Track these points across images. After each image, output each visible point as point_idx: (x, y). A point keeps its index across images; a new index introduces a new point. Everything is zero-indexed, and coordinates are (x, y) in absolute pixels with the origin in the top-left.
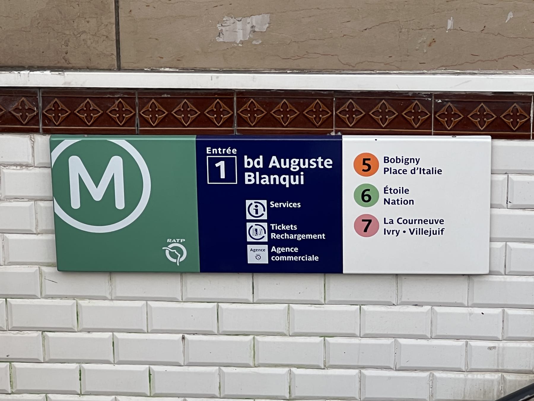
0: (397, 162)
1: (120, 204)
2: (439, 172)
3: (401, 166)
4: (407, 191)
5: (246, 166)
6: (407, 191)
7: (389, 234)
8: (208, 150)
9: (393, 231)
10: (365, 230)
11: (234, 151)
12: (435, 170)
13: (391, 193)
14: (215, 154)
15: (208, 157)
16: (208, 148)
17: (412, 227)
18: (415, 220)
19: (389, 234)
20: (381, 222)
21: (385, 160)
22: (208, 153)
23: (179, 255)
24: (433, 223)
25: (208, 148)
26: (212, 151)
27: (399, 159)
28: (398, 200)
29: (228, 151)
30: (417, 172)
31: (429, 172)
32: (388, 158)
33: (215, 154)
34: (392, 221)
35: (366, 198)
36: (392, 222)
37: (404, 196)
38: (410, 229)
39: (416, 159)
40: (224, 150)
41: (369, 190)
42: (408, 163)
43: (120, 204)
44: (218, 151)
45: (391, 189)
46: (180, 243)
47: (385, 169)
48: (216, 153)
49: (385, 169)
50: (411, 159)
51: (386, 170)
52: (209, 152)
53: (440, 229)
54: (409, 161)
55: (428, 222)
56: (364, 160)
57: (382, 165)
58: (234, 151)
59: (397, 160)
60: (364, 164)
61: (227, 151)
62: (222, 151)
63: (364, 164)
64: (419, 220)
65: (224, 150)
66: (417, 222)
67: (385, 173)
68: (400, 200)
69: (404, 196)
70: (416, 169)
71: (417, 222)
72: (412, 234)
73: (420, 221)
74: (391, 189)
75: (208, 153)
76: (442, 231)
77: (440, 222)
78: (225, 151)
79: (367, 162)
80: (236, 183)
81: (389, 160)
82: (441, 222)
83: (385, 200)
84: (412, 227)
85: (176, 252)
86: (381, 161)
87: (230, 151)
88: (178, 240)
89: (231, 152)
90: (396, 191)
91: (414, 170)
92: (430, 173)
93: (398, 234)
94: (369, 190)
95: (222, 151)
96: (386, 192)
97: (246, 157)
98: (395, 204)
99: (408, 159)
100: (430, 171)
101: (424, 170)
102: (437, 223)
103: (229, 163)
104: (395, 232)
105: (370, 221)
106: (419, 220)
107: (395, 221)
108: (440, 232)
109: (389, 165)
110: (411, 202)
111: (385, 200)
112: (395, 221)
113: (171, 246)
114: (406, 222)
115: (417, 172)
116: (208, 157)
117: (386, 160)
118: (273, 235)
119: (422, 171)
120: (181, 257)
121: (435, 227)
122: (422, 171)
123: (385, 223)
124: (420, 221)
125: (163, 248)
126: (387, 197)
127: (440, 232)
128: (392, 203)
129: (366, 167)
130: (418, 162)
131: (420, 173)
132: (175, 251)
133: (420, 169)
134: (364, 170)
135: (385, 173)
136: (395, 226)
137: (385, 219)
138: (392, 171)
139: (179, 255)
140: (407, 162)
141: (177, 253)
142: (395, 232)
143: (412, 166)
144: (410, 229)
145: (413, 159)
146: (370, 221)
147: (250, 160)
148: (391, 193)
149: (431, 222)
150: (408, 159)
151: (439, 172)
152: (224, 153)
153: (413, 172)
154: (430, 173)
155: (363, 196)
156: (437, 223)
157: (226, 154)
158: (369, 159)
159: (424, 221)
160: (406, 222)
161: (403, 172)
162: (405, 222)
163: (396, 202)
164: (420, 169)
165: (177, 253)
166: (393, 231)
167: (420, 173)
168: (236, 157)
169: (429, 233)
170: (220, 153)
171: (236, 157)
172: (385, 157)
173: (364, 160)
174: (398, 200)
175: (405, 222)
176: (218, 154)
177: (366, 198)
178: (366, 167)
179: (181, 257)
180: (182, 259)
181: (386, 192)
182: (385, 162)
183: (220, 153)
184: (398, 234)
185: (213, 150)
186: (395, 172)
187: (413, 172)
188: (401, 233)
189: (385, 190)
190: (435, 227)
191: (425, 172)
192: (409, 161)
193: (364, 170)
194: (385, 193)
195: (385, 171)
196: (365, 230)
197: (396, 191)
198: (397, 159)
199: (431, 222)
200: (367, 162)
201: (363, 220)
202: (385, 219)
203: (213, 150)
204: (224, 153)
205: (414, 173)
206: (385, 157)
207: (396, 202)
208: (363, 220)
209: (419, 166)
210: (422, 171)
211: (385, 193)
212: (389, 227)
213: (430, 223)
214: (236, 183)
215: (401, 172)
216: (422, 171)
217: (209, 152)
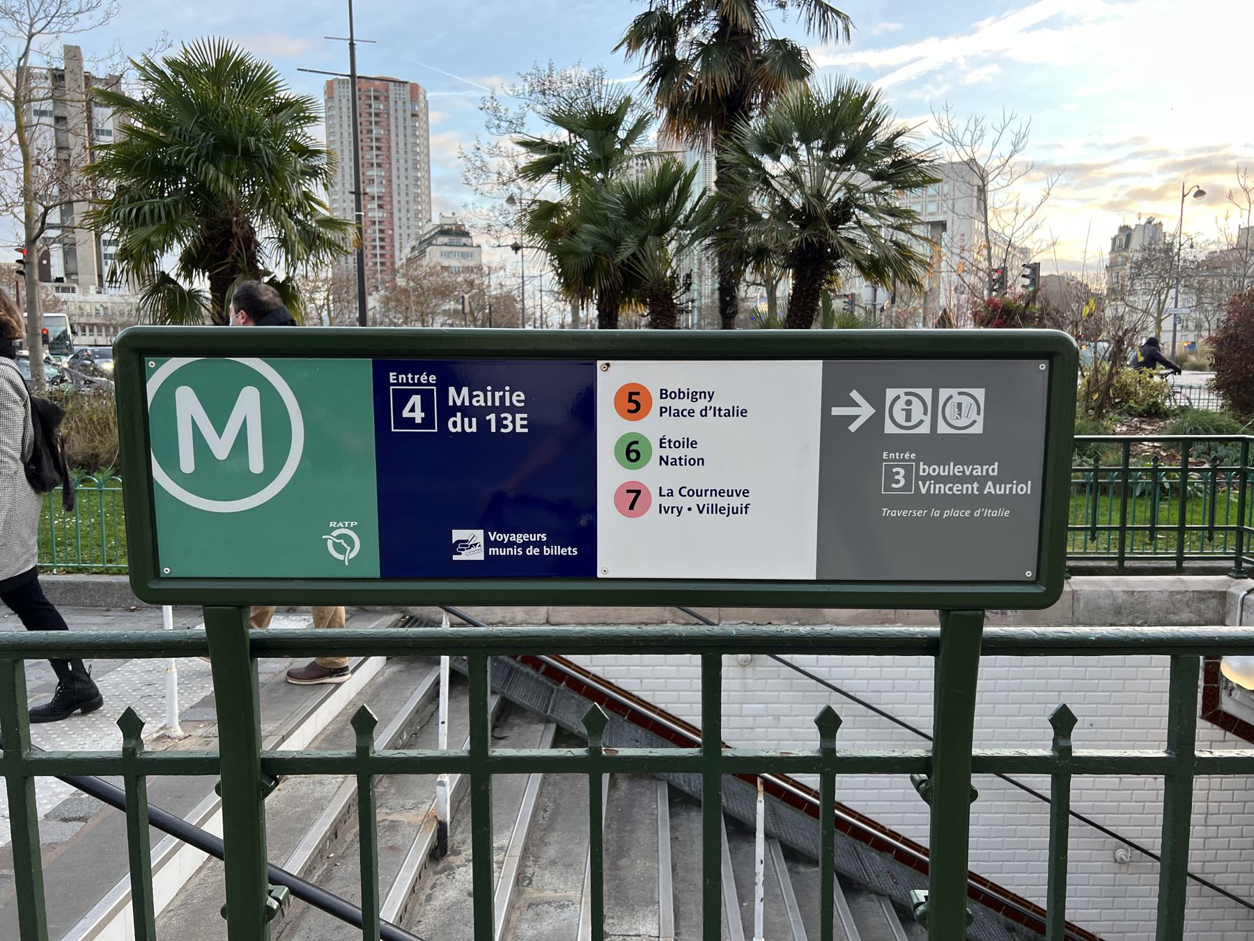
0: (679, 398)
1: (256, 464)
2: (743, 413)
3: (686, 404)
4: (694, 444)
5: (921, 473)
6: (694, 444)
7: (666, 512)
8: (391, 377)
9: (673, 508)
10: (631, 507)
11: (433, 378)
13: (670, 447)
14: (403, 384)
15: (391, 388)
16: (391, 374)
17: (702, 501)
18: (706, 491)
19: (666, 512)
20: (655, 493)
21: (662, 394)
22: (392, 381)
23: (349, 548)
24: (732, 496)
25: (391, 374)
26: (397, 379)
27: (683, 392)
28: (680, 459)
29: (424, 378)
30: (710, 413)
31: (728, 414)
32: (667, 391)
33: (403, 384)
34: (672, 493)
35: (633, 456)
36: (671, 494)
37: (690, 453)
38: (698, 505)
39: (709, 393)
40: (416, 377)
41: (636, 443)
42: (697, 399)
43: (256, 464)
44: (407, 379)
45: (670, 441)
46: (349, 528)
47: (661, 408)
48: (405, 381)
49: (661, 408)
50: (701, 393)
51: (664, 410)
52: (394, 379)
53: (744, 506)
54: (698, 396)
55: (726, 494)
56: (631, 394)
57: (657, 402)
58: (433, 378)
59: (680, 394)
60: (630, 400)
61: (422, 379)
62: (413, 379)
63: (630, 400)
64: (712, 491)
65: (416, 377)
66: (709, 493)
67: (661, 416)
68: (684, 458)
69: (690, 453)
70: (708, 408)
71: (709, 493)
72: (701, 512)
73: (714, 492)
74: (670, 441)
75: (392, 381)
76: (746, 507)
77: (744, 493)
78: (419, 379)
79: (634, 397)
80: (436, 431)
81: (668, 394)
82: (745, 493)
83: (661, 458)
84: (702, 501)
85: (343, 544)
86: (655, 395)
87: (426, 378)
88: (347, 523)
89: (428, 380)
90: (678, 444)
91: (706, 410)
92: (729, 416)
93: (680, 513)
94: (636, 443)
95: (413, 379)
96: (663, 445)
97: (922, 463)
98: (676, 464)
99: (696, 393)
100: (729, 413)
101: (720, 410)
102: (738, 495)
103: (908, 469)
104: (675, 510)
105: (638, 492)
106: (712, 491)
107: (676, 493)
108: (744, 510)
109: (667, 403)
110: (701, 461)
111: (661, 458)
112: (676, 493)
113: (335, 533)
114: (693, 493)
115: (710, 413)
116: (391, 388)
117: (664, 394)
118: (492, 551)
119: (717, 411)
120: (350, 552)
121: (736, 502)
122: (717, 412)
123: (661, 495)
124: (714, 492)
125: (324, 537)
126: (665, 452)
127: (744, 510)
128: (671, 464)
129: (633, 406)
130: (711, 398)
131: (715, 416)
132: (342, 541)
133: (715, 408)
134: (629, 411)
135: (661, 416)
136: (676, 501)
137: (661, 488)
138: (673, 412)
139: (349, 548)
140: (694, 397)
141: (345, 545)
142: (675, 510)
143: (702, 403)
144: (698, 505)
145: (705, 393)
146: (638, 492)
147: (926, 467)
148: (670, 447)
149: (730, 494)
150: (696, 393)
151: (743, 413)
152: (416, 382)
153: (704, 413)
154: (729, 416)
155: (628, 452)
156: (738, 495)
157: (420, 383)
158: (638, 394)
159: (720, 493)
160: (693, 493)
161: (689, 413)
162: (691, 493)
163: (678, 461)
164: (715, 408)
165: (345, 545)
166: (673, 508)
167: (715, 416)
168: (435, 388)
169: (726, 512)
170: (410, 381)
171: (435, 388)
172: (662, 390)
173: (631, 394)
174: (680, 459)
175: (691, 493)
176: (408, 384)
177: (633, 456)
178: (633, 406)
179: (350, 552)
180: (352, 555)
181: (663, 445)
182: (661, 398)
183: (410, 381)
184: (680, 513)
185: (400, 376)
186: (678, 413)
187: (704, 413)
188: (685, 511)
189: (661, 443)
190: (736, 502)
191: (722, 413)
192: (698, 396)
193: (629, 411)
194: (661, 447)
195: (661, 412)
196: (631, 507)
197: (678, 444)
198: (680, 392)
199: (730, 494)
200: (634, 397)
201: (628, 491)
202: (661, 488)
203: (400, 376)
204: (416, 382)
205: (706, 415)
206: (662, 390)
207: (678, 461)
208: (628, 491)
209: (712, 404)
210: (717, 412)
211: (661, 447)
212: (667, 502)
213: (728, 496)
214: (436, 431)
215: (685, 413)
216: (717, 411)
217: (394, 379)
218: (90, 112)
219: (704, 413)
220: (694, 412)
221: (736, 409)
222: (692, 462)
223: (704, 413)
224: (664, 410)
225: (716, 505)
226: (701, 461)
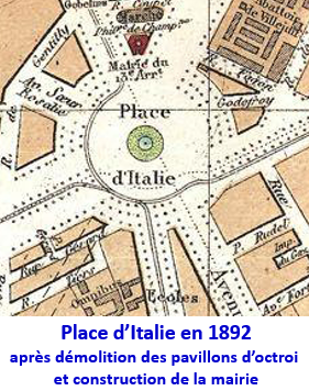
2: (14, 359)
12: (162, 178)
30: (127, 334)
47: (64, 327)
49: (64, 327)
51: (67, 329)
91: (122, 332)
100: (151, 334)
102: (193, 361)
110: (197, 334)
115: (127, 334)
122: (136, 333)
151: (14, 359)
161: (100, 334)
163: (218, 332)
191: (143, 334)
194: (213, 379)
195: (64, 333)
205: (122, 337)
207: (218, 332)
210: (136, 333)
211: (213, 379)
218: (108, 191)
219: (119, 334)
220: (106, 333)
221: (160, 329)
222: (216, 359)
223: (119, 334)
224: (67, 329)
225: (162, 327)
226: (197, 334)
